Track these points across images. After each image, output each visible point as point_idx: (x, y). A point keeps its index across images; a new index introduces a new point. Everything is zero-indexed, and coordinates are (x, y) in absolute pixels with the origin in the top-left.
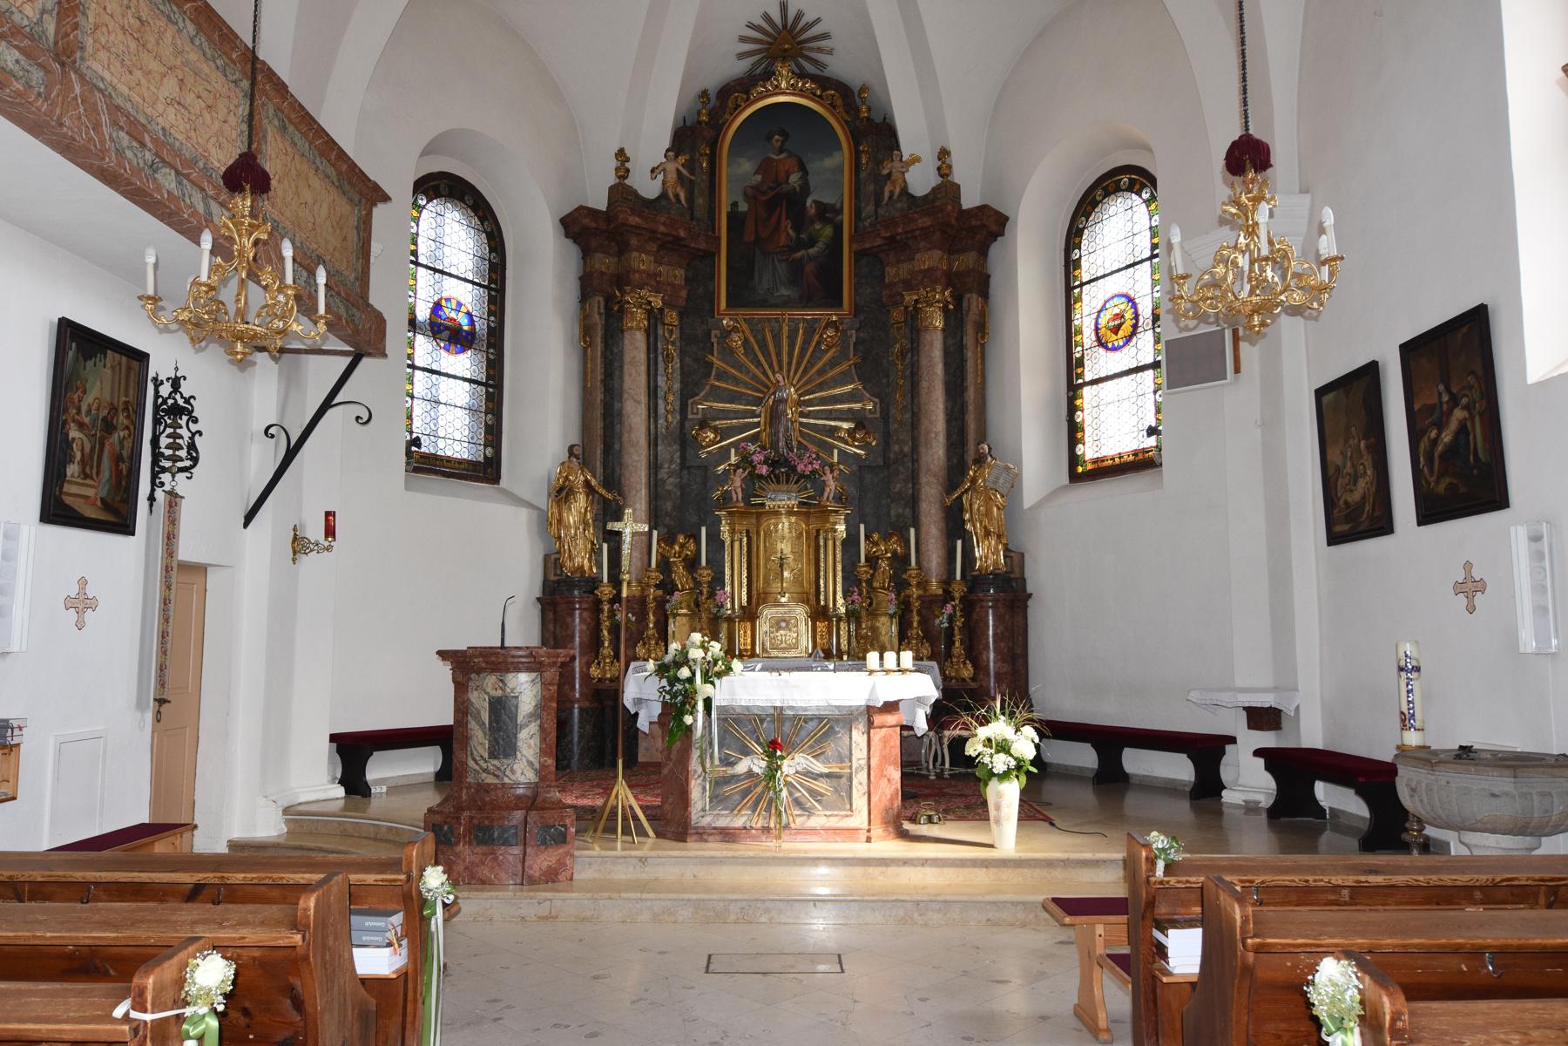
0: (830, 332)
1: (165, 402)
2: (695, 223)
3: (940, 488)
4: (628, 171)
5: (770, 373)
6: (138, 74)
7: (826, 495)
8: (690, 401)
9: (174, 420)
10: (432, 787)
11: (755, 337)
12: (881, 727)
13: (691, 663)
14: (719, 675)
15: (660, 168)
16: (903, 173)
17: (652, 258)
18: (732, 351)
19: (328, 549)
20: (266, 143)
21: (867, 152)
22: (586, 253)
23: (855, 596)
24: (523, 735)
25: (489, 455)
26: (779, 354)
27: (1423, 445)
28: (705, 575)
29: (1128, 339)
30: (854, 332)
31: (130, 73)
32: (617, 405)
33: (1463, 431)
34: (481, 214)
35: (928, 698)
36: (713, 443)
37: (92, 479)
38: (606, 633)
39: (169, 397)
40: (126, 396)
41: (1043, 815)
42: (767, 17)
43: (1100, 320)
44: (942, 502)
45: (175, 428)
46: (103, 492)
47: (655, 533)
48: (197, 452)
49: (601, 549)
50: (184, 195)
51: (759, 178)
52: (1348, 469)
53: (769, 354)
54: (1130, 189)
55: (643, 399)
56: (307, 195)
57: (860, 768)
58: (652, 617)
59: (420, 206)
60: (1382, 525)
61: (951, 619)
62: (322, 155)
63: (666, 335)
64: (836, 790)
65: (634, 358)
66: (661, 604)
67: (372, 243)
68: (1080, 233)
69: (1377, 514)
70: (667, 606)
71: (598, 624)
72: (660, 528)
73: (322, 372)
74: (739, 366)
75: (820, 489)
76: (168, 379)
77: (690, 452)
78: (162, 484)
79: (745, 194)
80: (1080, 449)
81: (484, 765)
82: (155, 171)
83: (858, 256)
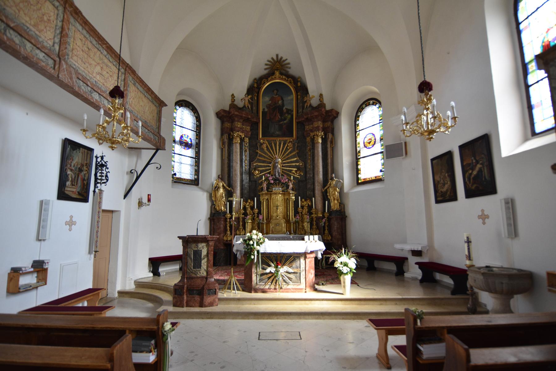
0: (290, 144)
1: (99, 163)
2: (253, 114)
3: (321, 187)
4: (235, 100)
5: (273, 155)
6: (87, 64)
7: (289, 189)
8: (252, 163)
9: (102, 168)
10: (178, 272)
11: (269, 145)
12: (309, 258)
13: (253, 240)
14: (261, 243)
15: (244, 99)
16: (310, 100)
17: (241, 124)
18: (263, 149)
19: (148, 205)
20: (129, 88)
21: (300, 95)
22: (223, 123)
23: (298, 217)
24: (203, 262)
25: (196, 178)
26: (276, 150)
27: (467, 175)
28: (256, 211)
29: (373, 146)
30: (297, 144)
31: (85, 64)
32: (231, 164)
33: (480, 171)
34: (194, 111)
35: (323, 249)
36: (258, 174)
37: (75, 186)
38: (228, 228)
39: (100, 162)
40: (87, 161)
41: (355, 282)
42: (272, 58)
43: (365, 140)
44: (322, 190)
45: (102, 171)
46: (79, 190)
47: (242, 199)
48: (108, 178)
49: (227, 204)
50: (101, 101)
51: (270, 102)
52: (442, 181)
53: (273, 150)
54: (373, 104)
55: (239, 162)
56: (141, 103)
57: (303, 270)
58: (241, 223)
59: (177, 109)
60: (453, 198)
61: (325, 223)
62: (147, 92)
63: (245, 144)
64: (296, 277)
65: (236, 151)
66: (244, 219)
67: (162, 118)
68: (359, 117)
69: (451, 195)
70: (245, 220)
71: (226, 225)
72: (243, 198)
73: (147, 155)
74: (265, 153)
75: (288, 187)
76: (100, 156)
77: (252, 177)
78: (98, 187)
79: (267, 106)
80: (359, 176)
81: (191, 271)
82: (92, 93)
83: (298, 123)
